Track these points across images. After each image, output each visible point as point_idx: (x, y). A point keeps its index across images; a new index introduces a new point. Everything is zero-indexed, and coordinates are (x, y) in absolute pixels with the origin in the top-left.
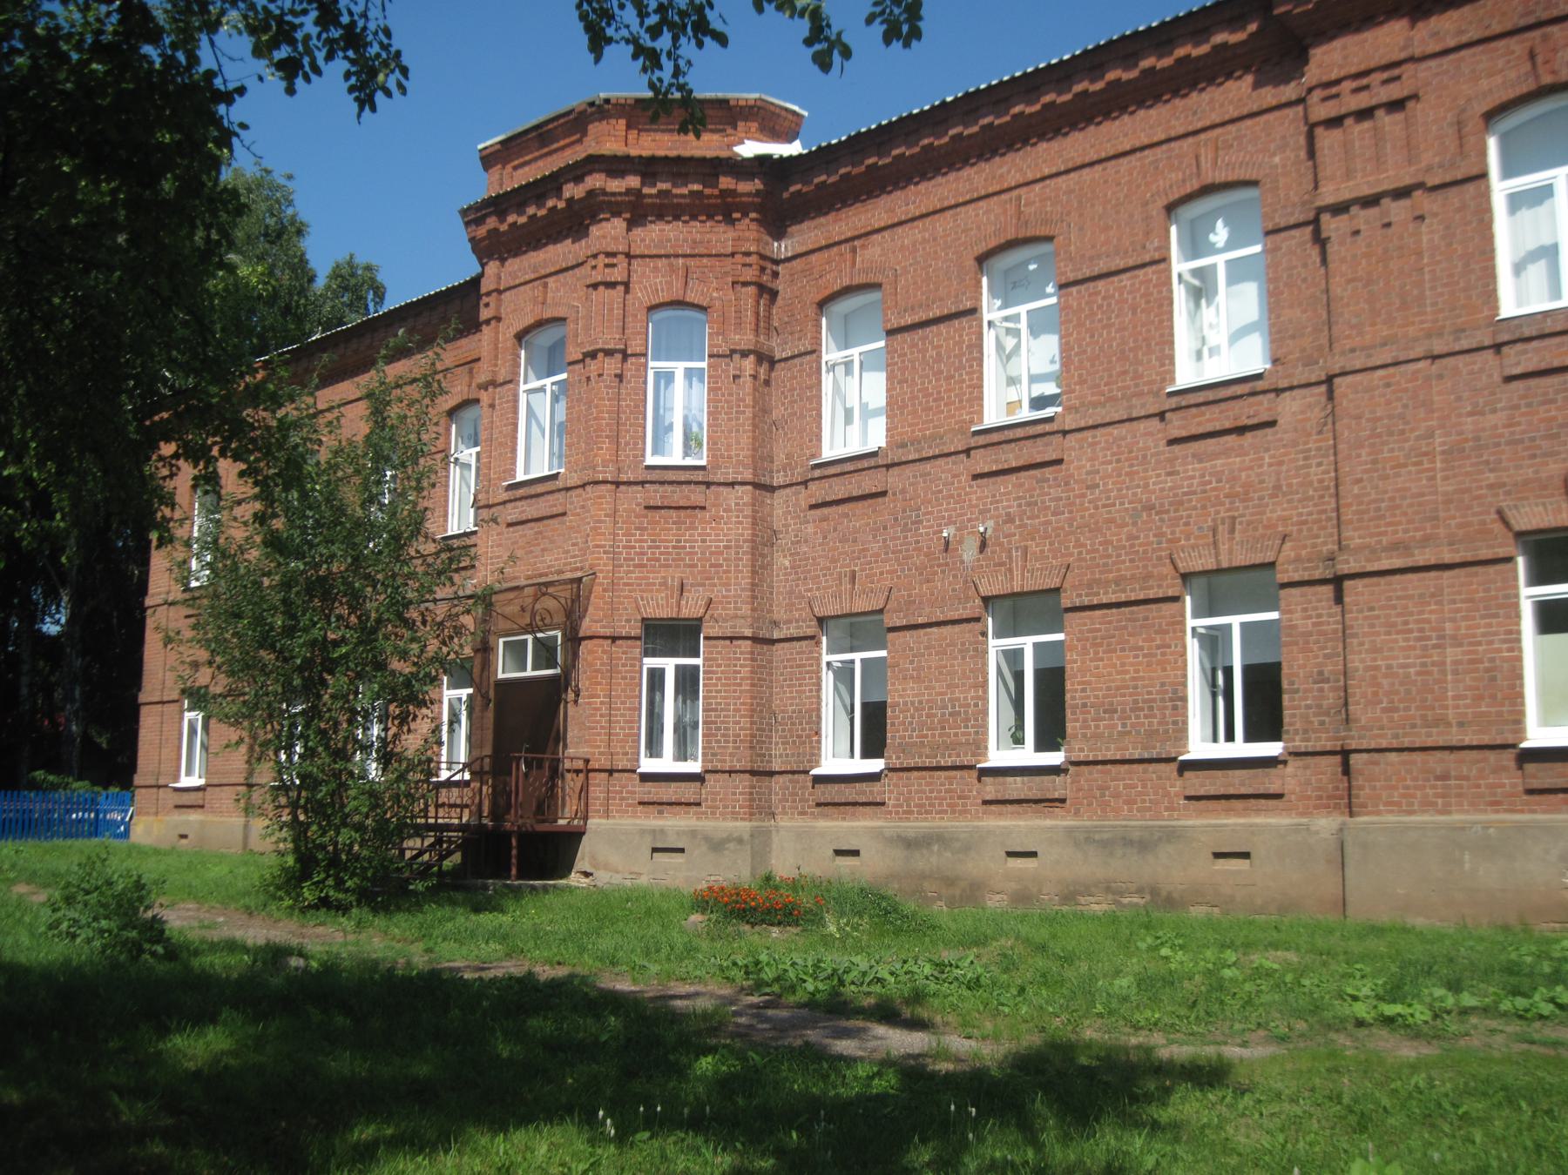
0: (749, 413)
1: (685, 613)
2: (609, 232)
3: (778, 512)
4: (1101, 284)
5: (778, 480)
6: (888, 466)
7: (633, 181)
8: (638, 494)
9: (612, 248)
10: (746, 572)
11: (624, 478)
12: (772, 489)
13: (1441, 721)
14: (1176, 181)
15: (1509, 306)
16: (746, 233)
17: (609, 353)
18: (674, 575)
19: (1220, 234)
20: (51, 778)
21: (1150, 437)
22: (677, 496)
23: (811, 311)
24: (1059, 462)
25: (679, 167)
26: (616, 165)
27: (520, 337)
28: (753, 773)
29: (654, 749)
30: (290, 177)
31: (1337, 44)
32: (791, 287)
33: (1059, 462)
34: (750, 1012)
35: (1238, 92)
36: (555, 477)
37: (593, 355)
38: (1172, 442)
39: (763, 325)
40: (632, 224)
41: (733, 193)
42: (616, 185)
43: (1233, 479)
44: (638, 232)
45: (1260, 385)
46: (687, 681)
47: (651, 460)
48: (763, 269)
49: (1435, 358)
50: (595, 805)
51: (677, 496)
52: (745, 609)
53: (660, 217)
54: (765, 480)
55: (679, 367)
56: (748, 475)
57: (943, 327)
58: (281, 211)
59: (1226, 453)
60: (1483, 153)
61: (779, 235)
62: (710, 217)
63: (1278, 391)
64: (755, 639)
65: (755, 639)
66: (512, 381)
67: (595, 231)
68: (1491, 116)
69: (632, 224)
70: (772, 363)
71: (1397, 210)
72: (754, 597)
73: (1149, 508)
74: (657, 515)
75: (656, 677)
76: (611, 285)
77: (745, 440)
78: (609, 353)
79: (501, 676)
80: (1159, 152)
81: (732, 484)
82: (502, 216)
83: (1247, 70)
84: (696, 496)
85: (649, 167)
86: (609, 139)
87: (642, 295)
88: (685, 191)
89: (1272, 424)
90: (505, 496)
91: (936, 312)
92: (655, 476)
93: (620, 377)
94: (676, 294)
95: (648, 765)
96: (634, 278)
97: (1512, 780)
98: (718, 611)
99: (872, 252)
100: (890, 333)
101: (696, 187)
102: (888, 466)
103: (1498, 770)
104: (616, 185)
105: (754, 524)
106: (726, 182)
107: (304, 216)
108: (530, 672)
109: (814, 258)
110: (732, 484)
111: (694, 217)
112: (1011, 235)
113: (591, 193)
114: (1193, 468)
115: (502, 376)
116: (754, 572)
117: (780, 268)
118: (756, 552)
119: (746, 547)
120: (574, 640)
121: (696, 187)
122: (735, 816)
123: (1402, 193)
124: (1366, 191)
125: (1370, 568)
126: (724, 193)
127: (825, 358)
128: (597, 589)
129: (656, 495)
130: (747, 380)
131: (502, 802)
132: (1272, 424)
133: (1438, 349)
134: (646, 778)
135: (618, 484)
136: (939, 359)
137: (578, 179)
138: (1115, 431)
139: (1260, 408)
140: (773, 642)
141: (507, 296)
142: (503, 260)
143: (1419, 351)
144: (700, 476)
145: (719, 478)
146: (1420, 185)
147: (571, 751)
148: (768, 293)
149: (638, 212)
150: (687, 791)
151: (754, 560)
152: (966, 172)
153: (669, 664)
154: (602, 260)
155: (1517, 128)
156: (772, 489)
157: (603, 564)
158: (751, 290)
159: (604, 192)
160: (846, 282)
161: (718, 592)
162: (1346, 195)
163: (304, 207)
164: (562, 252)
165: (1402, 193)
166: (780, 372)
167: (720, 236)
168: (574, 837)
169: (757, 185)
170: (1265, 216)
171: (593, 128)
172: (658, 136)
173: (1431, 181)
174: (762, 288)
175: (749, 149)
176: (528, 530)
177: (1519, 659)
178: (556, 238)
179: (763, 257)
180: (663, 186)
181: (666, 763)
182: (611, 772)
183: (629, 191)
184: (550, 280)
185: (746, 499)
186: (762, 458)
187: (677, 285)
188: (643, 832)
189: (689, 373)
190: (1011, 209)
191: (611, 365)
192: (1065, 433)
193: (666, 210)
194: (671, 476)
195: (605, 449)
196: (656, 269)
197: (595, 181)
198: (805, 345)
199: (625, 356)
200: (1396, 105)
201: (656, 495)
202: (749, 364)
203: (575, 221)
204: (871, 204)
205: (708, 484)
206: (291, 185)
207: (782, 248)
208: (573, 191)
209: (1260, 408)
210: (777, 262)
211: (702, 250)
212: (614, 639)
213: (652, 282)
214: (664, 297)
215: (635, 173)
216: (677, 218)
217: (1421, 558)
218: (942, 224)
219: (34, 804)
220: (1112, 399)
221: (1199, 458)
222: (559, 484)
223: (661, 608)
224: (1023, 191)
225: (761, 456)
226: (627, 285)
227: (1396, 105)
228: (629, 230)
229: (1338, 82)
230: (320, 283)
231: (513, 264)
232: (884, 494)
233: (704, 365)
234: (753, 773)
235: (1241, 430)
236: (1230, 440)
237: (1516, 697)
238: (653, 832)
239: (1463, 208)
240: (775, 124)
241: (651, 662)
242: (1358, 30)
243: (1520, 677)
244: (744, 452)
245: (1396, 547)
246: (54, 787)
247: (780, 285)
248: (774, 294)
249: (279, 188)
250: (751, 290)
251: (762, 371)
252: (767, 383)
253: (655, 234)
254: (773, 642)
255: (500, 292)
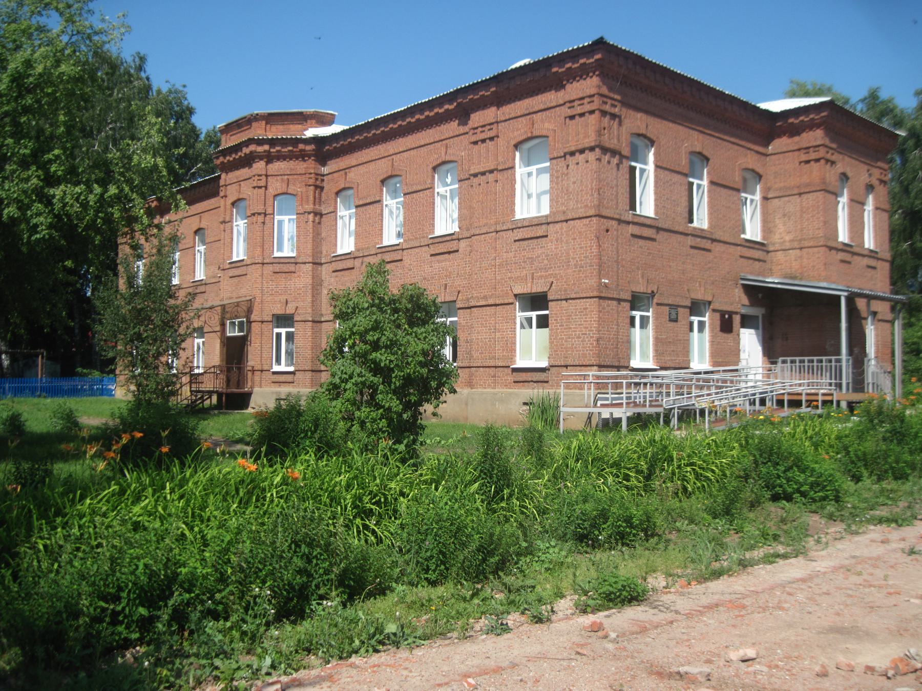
0: (311, 235)
1: (288, 312)
2: (259, 166)
3: (324, 273)
4: (414, 195)
5: (323, 261)
6: (355, 258)
7: (266, 147)
8: (271, 267)
9: (260, 173)
10: (310, 296)
11: (265, 261)
12: (321, 264)
13: (494, 358)
14: (435, 159)
15: (518, 216)
16: (309, 165)
17: (259, 214)
18: (283, 298)
19: (449, 180)
20: (85, 371)
21: (425, 253)
22: (285, 268)
23: (333, 196)
24: (401, 260)
25: (284, 142)
26: (260, 142)
27: (233, 204)
28: (312, 371)
29: (278, 361)
30: (184, 86)
31: (477, 113)
32: (330, 187)
33: (401, 260)
34: (870, 562)
35: (453, 127)
36: (243, 260)
37: (254, 214)
38: (432, 255)
39: (317, 200)
40: (267, 163)
41: (304, 150)
42: (260, 149)
43: (447, 270)
44: (270, 166)
45: (454, 237)
46: (290, 337)
47: (277, 254)
48: (317, 179)
49: (497, 232)
50: (257, 383)
51: (285, 268)
52: (310, 310)
53: (278, 160)
54: (318, 261)
55: (286, 218)
56: (310, 260)
57: (371, 206)
58: (181, 102)
59: (445, 260)
60: (514, 159)
61: (324, 165)
62: (297, 159)
63: (459, 240)
64: (313, 321)
65: (313, 321)
66: (231, 221)
67: (255, 165)
68: (516, 146)
69: (267, 163)
70: (321, 215)
71: (491, 177)
72: (313, 306)
73: (425, 279)
74: (277, 275)
75: (279, 335)
76: (260, 187)
77: (310, 246)
78: (259, 214)
79: (228, 335)
80: (432, 146)
81: (305, 263)
82: (225, 156)
83: (456, 118)
84: (292, 268)
85: (272, 142)
86: (258, 131)
87: (271, 191)
88: (286, 150)
89: (457, 251)
90: (228, 266)
91: (368, 201)
92: (277, 261)
93: (264, 223)
94: (284, 190)
95: (276, 368)
96: (269, 184)
97: (511, 378)
98: (299, 311)
99: (352, 175)
100: (357, 207)
101: (290, 148)
102: (355, 258)
103: (507, 374)
104: (260, 149)
105: (313, 278)
106: (301, 146)
107: (193, 104)
108: (237, 334)
109: (335, 175)
110: (305, 263)
111: (291, 159)
112: (390, 174)
113: (251, 152)
114: (436, 265)
115: (227, 219)
116: (313, 296)
117: (325, 178)
118: (313, 288)
119: (310, 287)
120: (249, 322)
121: (290, 148)
122: (306, 387)
123: (491, 172)
124: (482, 170)
125: (478, 304)
126: (301, 150)
127: (339, 214)
128: (256, 304)
129: (277, 268)
130: (310, 223)
131: (856, 350)
132: (457, 251)
133: (498, 229)
134: (274, 373)
135: (263, 264)
136: (370, 218)
137: (247, 146)
138: (417, 250)
139: (453, 246)
140: (321, 322)
141: (229, 187)
142: (227, 173)
143: (493, 229)
144: (293, 261)
145: (300, 261)
146: (496, 169)
147: (249, 363)
148: (319, 188)
149: (269, 158)
150: (289, 378)
151: (313, 292)
152: (379, 147)
153: (283, 331)
154: (257, 178)
155: (533, 147)
156: (321, 264)
157: (258, 293)
158: (312, 188)
159: (256, 152)
160: (343, 186)
161: (300, 304)
162: (477, 171)
163: (192, 100)
164: (244, 172)
165: (491, 172)
166: (324, 219)
167: (300, 166)
168: (249, 395)
169: (312, 147)
170: (459, 175)
171: (254, 124)
172: (278, 127)
173: (500, 168)
174: (316, 187)
175: (311, 133)
176: (236, 280)
177: (515, 337)
178: (243, 166)
179: (317, 174)
180: (278, 148)
181: (283, 368)
182: (262, 371)
183: (265, 151)
184: (242, 183)
185: (310, 269)
186: (317, 253)
187: (285, 186)
188: (273, 393)
189: (289, 220)
190: (390, 163)
191: (260, 219)
192: (403, 250)
193: (280, 157)
194: (282, 261)
195: (258, 251)
196: (277, 180)
197: (252, 148)
198: (331, 209)
199: (265, 215)
200: (491, 139)
201: (277, 268)
202: (311, 217)
203: (248, 161)
204: (351, 156)
205: (296, 263)
206: (185, 90)
207: (325, 170)
208: (246, 150)
209: (453, 246)
210: (323, 175)
211: (294, 172)
212: (262, 322)
213: (275, 185)
214: (279, 191)
215: (267, 144)
216: (285, 160)
217: (491, 302)
218: (372, 166)
219: (77, 383)
220: (416, 238)
221: (439, 262)
222: (244, 263)
223: (279, 310)
224: (394, 157)
225: (316, 252)
226: (266, 187)
227: (491, 139)
228: (267, 165)
229: (477, 128)
230: (202, 137)
231: (231, 175)
232: (353, 268)
233: (295, 217)
234: (312, 371)
235: (449, 253)
236: (446, 256)
237: (513, 350)
238: (277, 393)
239: (507, 178)
240: (324, 120)
241: (276, 330)
242: (483, 109)
243: (515, 343)
244: (309, 252)
245: (485, 298)
246: (85, 375)
247: (325, 184)
248: (322, 188)
249: (181, 92)
250: (312, 188)
251: (317, 219)
252: (319, 223)
253: (277, 166)
254: (321, 322)
255: (226, 186)
